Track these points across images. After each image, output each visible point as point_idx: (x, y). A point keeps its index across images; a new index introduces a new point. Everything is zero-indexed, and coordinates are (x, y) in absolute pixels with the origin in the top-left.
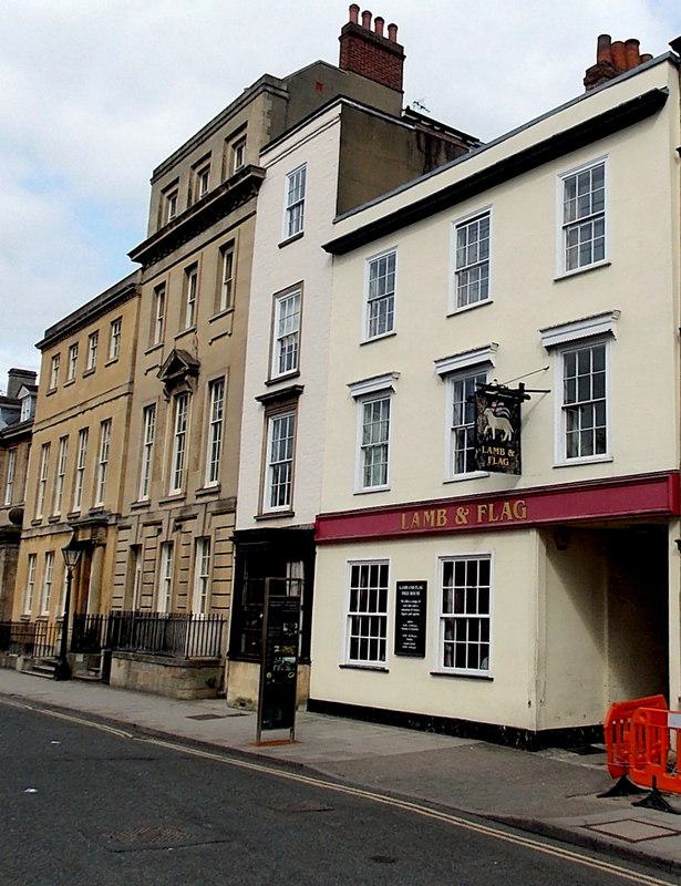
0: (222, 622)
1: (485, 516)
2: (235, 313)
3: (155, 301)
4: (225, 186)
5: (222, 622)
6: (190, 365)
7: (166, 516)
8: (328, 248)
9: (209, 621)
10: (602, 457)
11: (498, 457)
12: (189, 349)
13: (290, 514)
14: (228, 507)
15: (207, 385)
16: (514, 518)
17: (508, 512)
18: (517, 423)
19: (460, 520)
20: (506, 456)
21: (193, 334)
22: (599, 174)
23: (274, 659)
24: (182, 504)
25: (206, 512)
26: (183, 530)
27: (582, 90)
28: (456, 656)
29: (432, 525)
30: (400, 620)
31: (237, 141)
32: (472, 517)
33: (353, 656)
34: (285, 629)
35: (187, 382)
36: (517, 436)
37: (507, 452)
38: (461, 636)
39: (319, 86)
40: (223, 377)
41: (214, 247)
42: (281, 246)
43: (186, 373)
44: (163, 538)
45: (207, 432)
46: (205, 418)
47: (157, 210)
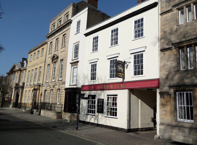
4: (51, 32)
8: (84, 35)
10: (142, 75)
12: (57, 54)
14: (64, 83)
20: (122, 75)
22: (142, 19)
41: (62, 35)
44: (51, 89)
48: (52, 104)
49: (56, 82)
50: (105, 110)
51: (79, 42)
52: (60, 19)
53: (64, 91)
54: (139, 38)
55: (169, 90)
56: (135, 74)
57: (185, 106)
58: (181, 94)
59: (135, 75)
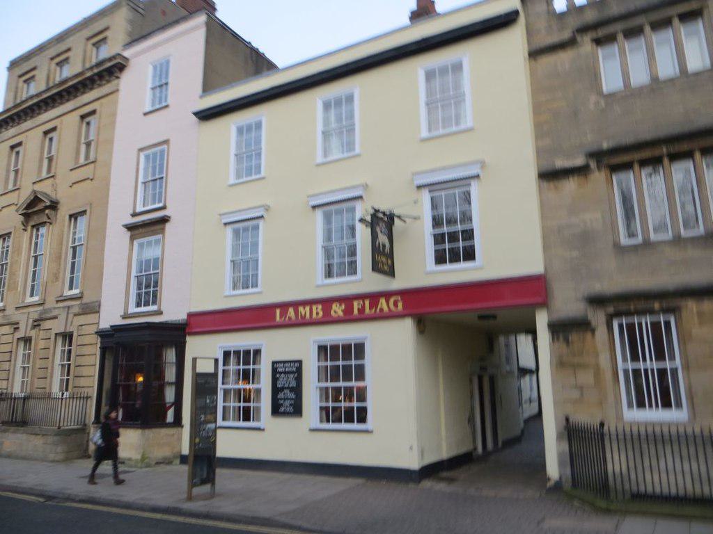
0: (87, 398)
2: (97, 164)
3: (10, 157)
4: (48, 89)
5: (87, 398)
6: (51, 201)
7: (24, 320)
8: (196, 114)
9: (70, 398)
10: (254, 290)
12: (48, 190)
13: (159, 313)
14: (93, 309)
15: (68, 217)
21: (52, 179)
22: (259, 125)
23: (202, 426)
24: (41, 308)
25: (68, 313)
26: (42, 327)
27: (406, 21)
28: (330, 415)
30: (276, 390)
31: (99, 39)
32: (348, 310)
34: (208, 401)
35: (47, 215)
38: (336, 399)
39: (164, 13)
40: (10, 233)
42: (145, 114)
43: (46, 207)
44: (20, 334)
45: (66, 253)
46: (64, 243)
47: (12, 88)
48: (31, 403)
49: (51, 303)
50: (312, 400)
51: (166, 142)
52: (58, 55)
53: (98, 341)
54: (249, 178)
55: (586, 310)
56: (440, 259)
59: (326, 277)
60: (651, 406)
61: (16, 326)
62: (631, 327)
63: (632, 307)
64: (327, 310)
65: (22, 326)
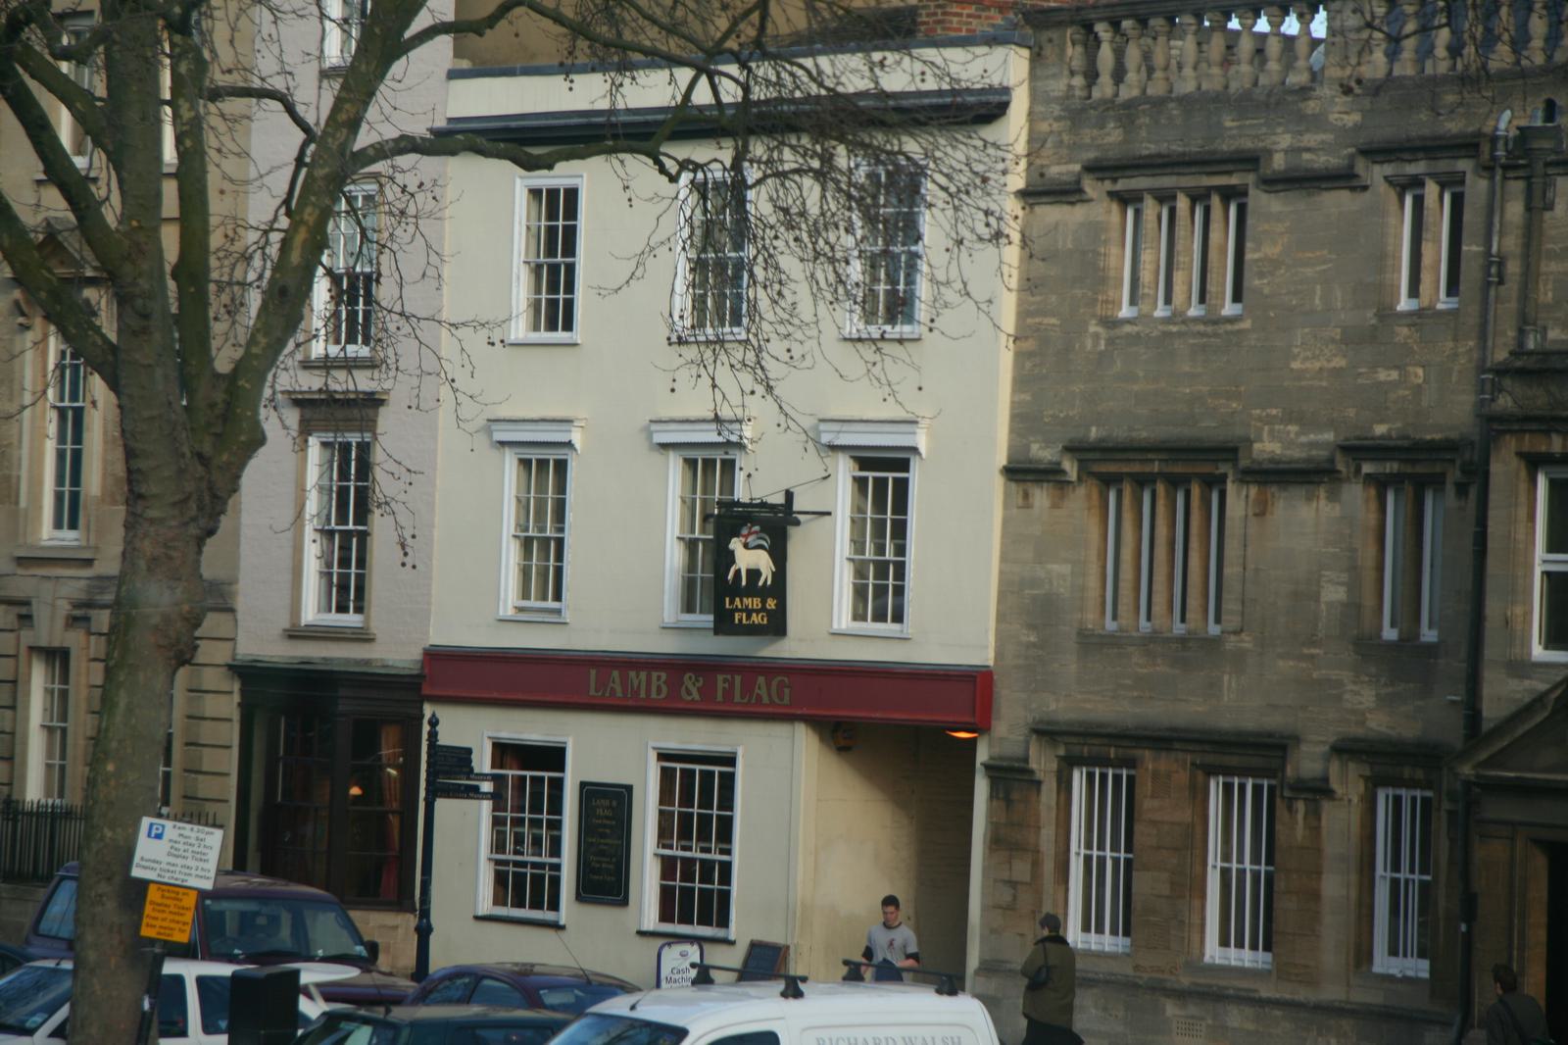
1: (728, 694)
11: (749, 612)
13: (362, 636)
16: (772, 703)
17: (763, 692)
18: (779, 555)
19: (689, 693)
20: (764, 609)
29: (643, 694)
33: (499, 900)
36: (780, 574)
37: (764, 602)
38: (688, 876)
57: (1248, 865)
58: (1228, 789)
60: (1405, 955)
61: (24, 611)
62: (1397, 800)
63: (1112, 753)
64: (675, 686)
65: (41, 613)
